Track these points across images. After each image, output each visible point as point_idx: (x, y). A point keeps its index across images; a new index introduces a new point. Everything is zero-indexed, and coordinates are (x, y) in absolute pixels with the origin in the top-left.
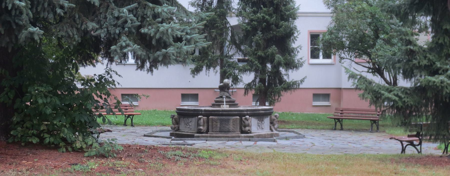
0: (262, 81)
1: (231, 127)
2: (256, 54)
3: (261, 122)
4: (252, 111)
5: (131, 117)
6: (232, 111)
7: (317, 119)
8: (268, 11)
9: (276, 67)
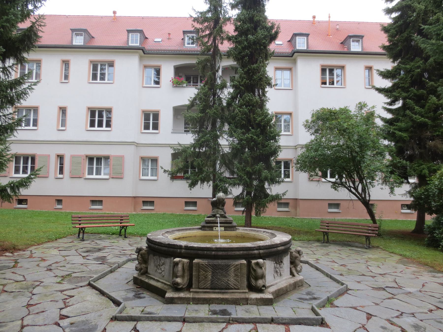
0: (249, 193)
1: (232, 280)
2: (245, 170)
3: (280, 265)
4: (267, 249)
5: (125, 228)
6: (233, 251)
7: (290, 225)
8: (256, 132)
9: (262, 182)
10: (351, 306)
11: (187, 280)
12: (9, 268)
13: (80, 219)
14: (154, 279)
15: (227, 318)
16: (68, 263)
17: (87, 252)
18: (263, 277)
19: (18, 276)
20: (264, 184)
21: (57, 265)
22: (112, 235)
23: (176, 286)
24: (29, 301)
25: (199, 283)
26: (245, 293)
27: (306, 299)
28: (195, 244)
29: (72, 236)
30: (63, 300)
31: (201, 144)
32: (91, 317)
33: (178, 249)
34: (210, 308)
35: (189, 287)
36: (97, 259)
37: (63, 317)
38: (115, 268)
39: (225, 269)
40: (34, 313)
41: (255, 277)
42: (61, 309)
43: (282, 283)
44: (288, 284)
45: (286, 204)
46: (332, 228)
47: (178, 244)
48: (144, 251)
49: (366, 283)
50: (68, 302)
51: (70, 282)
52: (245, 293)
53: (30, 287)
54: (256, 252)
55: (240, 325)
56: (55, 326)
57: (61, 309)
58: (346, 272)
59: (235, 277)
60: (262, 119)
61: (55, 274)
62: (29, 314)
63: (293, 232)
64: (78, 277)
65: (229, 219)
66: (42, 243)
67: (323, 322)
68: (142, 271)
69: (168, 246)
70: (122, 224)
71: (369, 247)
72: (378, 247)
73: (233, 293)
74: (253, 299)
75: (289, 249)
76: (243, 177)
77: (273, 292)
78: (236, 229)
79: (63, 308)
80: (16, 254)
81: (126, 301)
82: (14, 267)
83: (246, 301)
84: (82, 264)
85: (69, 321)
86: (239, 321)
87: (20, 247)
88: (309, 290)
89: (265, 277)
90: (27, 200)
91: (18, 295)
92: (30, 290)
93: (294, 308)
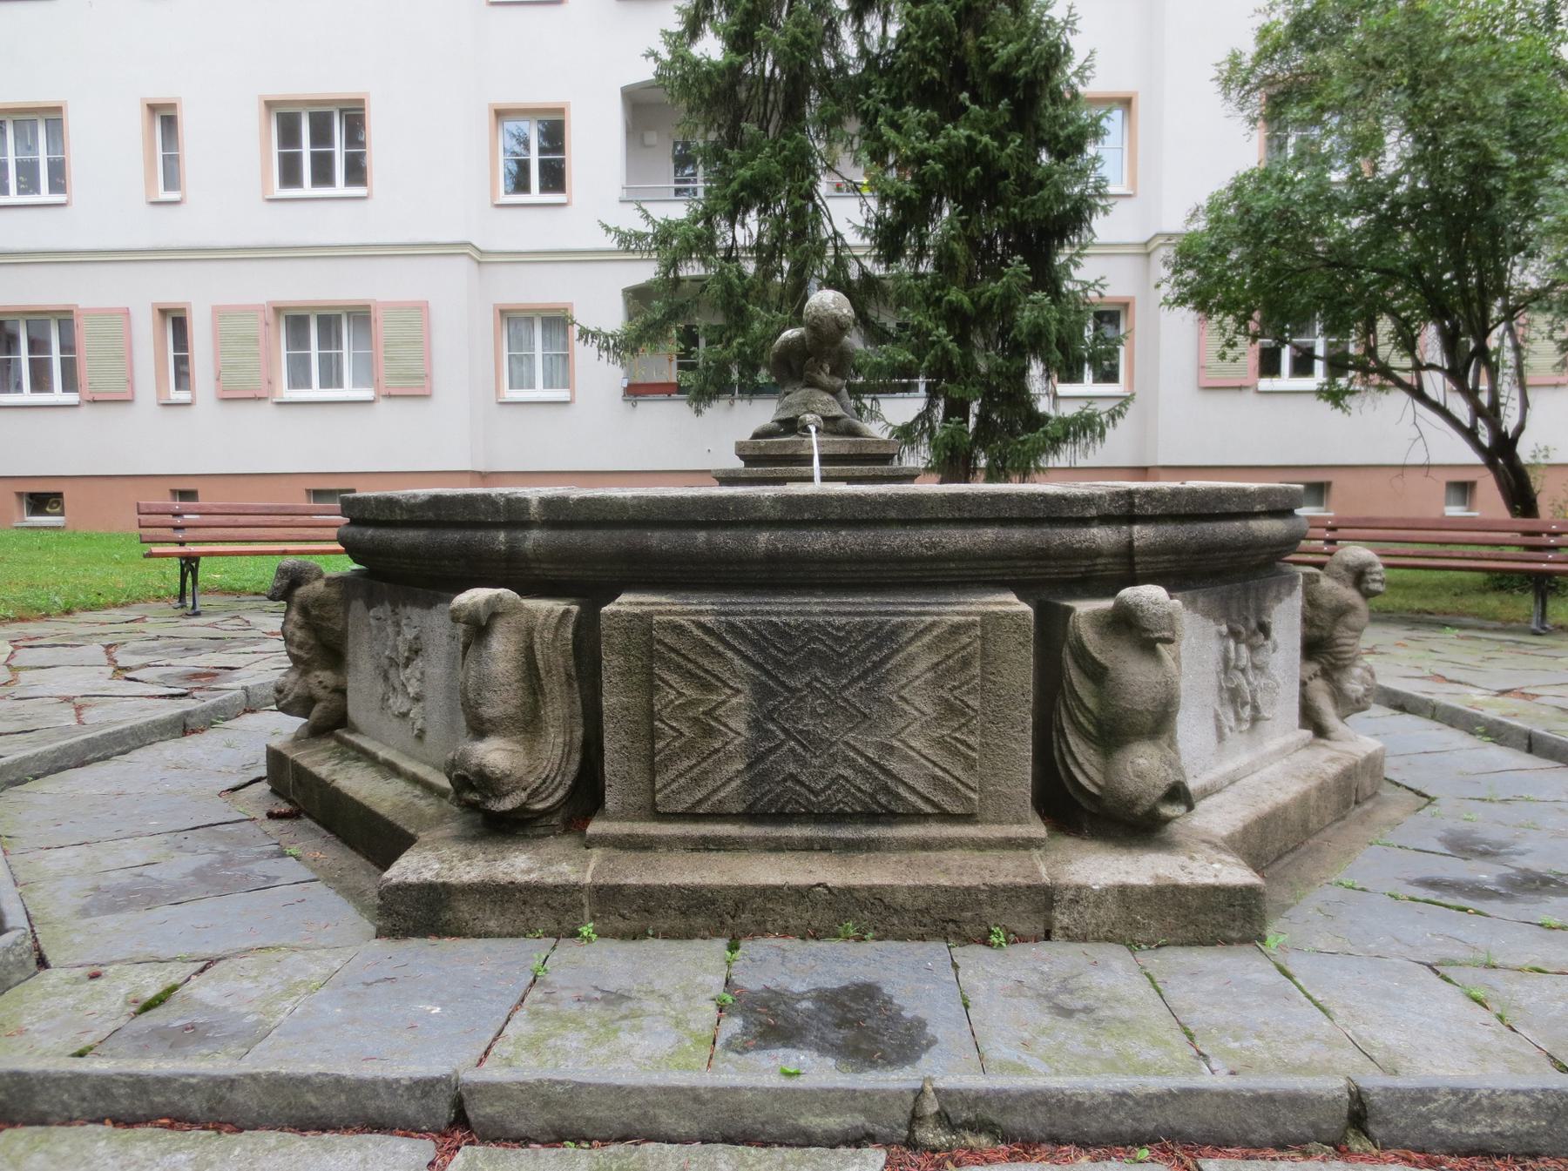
2: (939, 300)
8: (989, 121)
11: (566, 756)
13: (178, 521)
15: (886, 1097)
23: (474, 797)
25: (653, 772)
26: (1028, 844)
31: (735, 195)
33: (497, 526)
34: (738, 979)
41: (1099, 724)
43: (1267, 772)
44: (1313, 782)
52: (1028, 844)
54: (1103, 536)
59: (939, 720)
60: (1019, 54)
68: (317, 710)
69: (431, 515)
73: (925, 845)
74: (1100, 898)
76: (929, 333)
86: (1016, 1121)
90: (59, 495)
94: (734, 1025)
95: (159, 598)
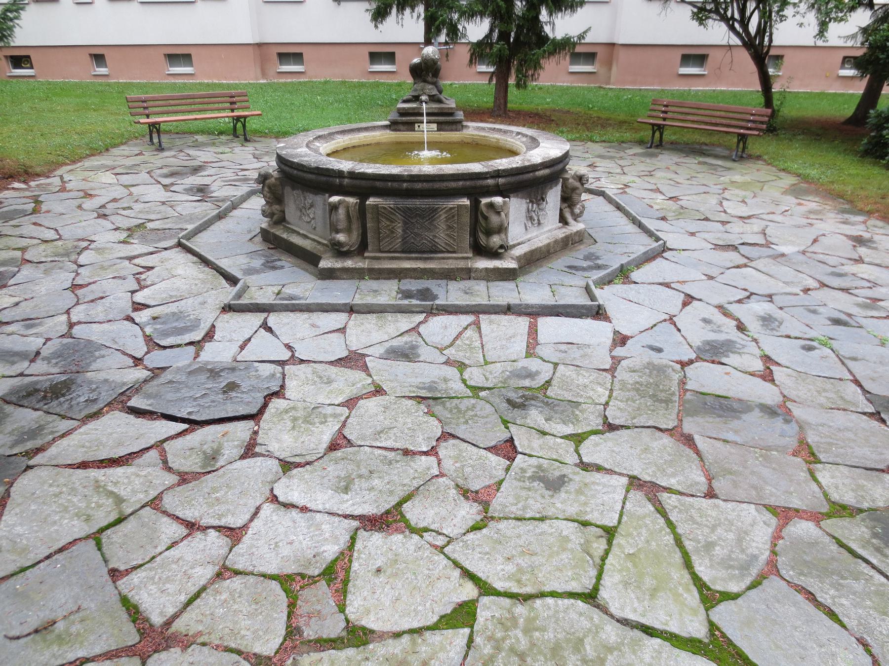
0: (504, 36)
1: (441, 235)
3: (538, 205)
6: (443, 181)
7: (591, 106)
10: (661, 281)
11: (358, 237)
12: (24, 214)
14: (298, 233)
16: (136, 201)
17: (172, 175)
18: (502, 229)
19: (47, 231)
20: (539, 13)
21: (116, 205)
22: (218, 135)
23: (337, 247)
24: (74, 279)
26: (467, 258)
27: (584, 269)
28: (368, 168)
29: (138, 141)
30: (133, 275)
32: (187, 305)
33: (336, 177)
34: (401, 287)
35: (362, 249)
36: (189, 191)
37: (139, 307)
38: (226, 209)
39: (429, 215)
40: (86, 300)
42: (133, 292)
43: (540, 238)
44: (553, 240)
45: (590, 57)
46: (676, 116)
47: (335, 168)
48: (273, 179)
49: (706, 236)
50: (145, 280)
51: (144, 240)
52: (467, 258)
53: (71, 252)
54: (490, 182)
55: (451, 317)
56: (126, 322)
57: (133, 292)
58: (673, 214)
59: (447, 230)
61: (113, 224)
62: (77, 303)
63: (594, 122)
64: (158, 230)
65: (447, 106)
66: (81, 159)
67: (600, 312)
68: (275, 217)
70: (236, 113)
71: (742, 157)
72: (759, 158)
73: (443, 258)
74: (481, 270)
75: (563, 170)
77: (520, 256)
78: (462, 126)
79: (137, 291)
80: (32, 184)
81: (250, 274)
82: (35, 211)
83: (468, 274)
84: (163, 203)
85: (149, 314)
87: (38, 170)
88: (592, 251)
89: (506, 229)
90: (28, 57)
91: (52, 268)
92: (73, 257)
93: (556, 284)
94: (400, 295)
95: (136, 138)
